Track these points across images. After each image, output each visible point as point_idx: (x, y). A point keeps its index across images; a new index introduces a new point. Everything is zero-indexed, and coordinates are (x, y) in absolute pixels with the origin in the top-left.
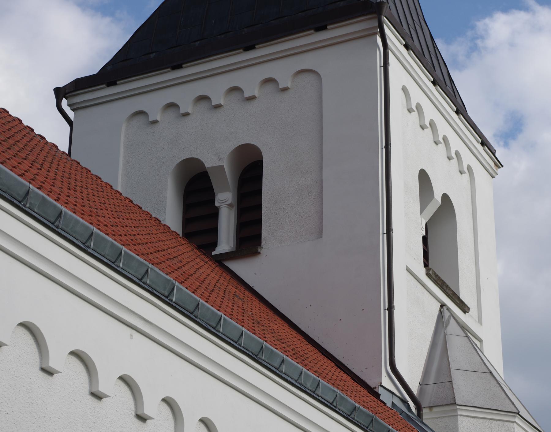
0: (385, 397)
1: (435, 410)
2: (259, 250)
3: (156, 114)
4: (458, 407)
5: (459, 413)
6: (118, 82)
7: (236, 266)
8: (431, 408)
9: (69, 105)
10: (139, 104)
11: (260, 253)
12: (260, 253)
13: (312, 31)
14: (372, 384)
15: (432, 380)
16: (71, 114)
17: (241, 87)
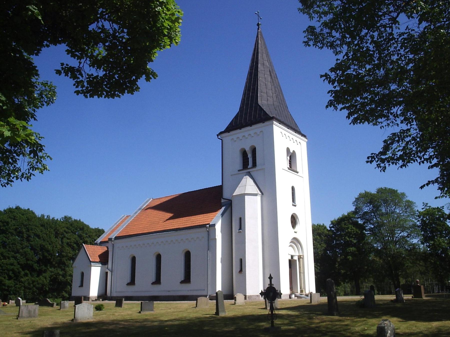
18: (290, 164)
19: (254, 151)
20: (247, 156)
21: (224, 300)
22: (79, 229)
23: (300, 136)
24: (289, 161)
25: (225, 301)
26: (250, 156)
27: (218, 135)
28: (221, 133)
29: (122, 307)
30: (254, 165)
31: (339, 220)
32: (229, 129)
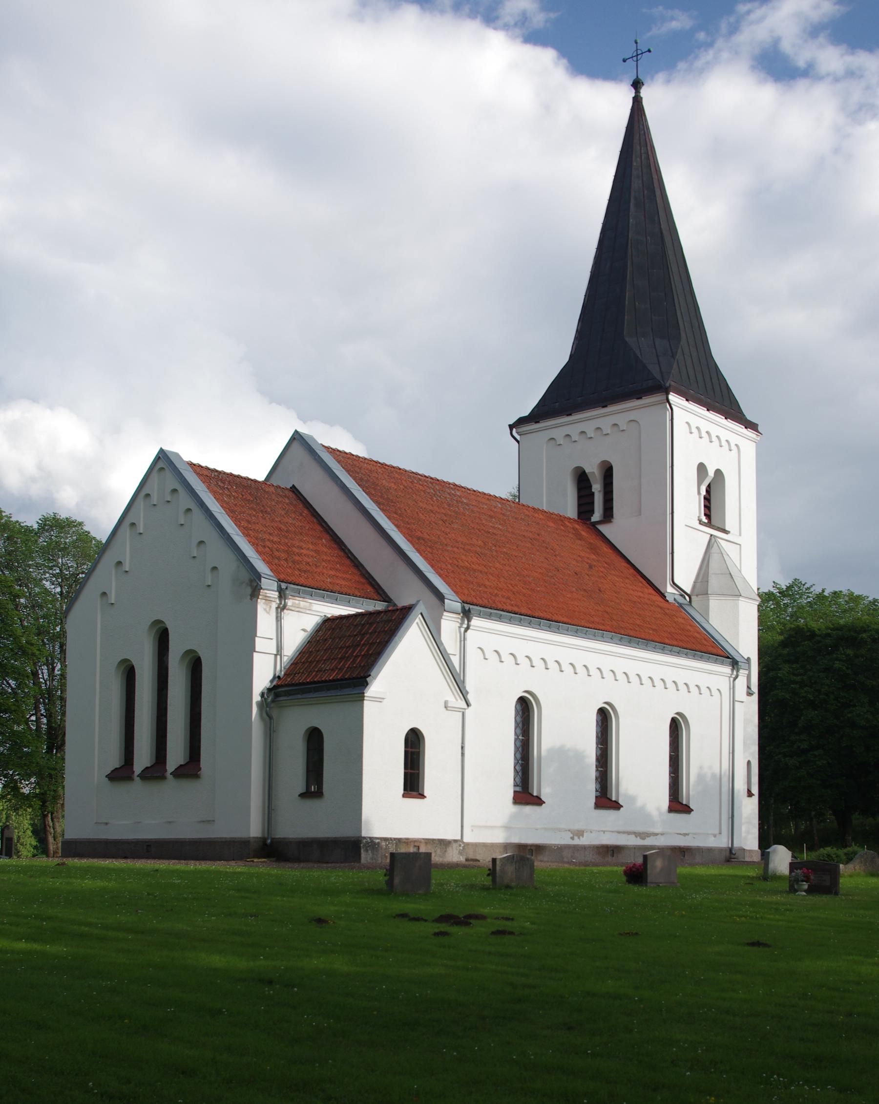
0: (670, 599)
1: (699, 596)
2: (612, 520)
3: (575, 437)
4: (710, 595)
5: (710, 598)
6: (643, 398)
7: (602, 528)
8: (697, 596)
9: (517, 433)
10: (553, 433)
11: (612, 522)
12: (612, 522)
13: (635, 400)
14: (663, 592)
15: (699, 581)
16: (518, 437)
17: (619, 424)
18: (708, 507)
19: (608, 472)
20: (591, 487)
21: (360, 862)
22: (756, 890)
23: (740, 429)
24: (705, 498)
25: (363, 860)
26: (597, 488)
27: (511, 427)
28: (521, 422)
29: (430, 851)
30: (608, 514)
31: (634, 869)
32: (543, 412)
